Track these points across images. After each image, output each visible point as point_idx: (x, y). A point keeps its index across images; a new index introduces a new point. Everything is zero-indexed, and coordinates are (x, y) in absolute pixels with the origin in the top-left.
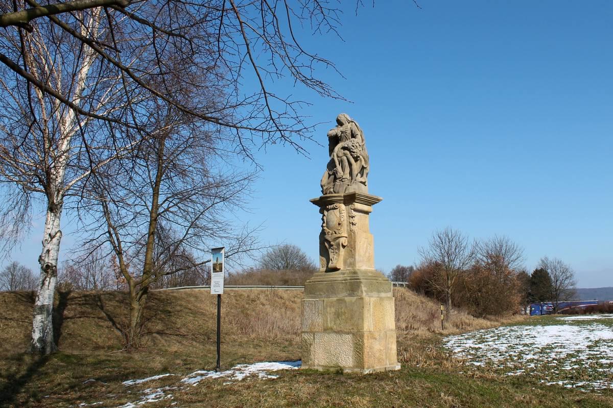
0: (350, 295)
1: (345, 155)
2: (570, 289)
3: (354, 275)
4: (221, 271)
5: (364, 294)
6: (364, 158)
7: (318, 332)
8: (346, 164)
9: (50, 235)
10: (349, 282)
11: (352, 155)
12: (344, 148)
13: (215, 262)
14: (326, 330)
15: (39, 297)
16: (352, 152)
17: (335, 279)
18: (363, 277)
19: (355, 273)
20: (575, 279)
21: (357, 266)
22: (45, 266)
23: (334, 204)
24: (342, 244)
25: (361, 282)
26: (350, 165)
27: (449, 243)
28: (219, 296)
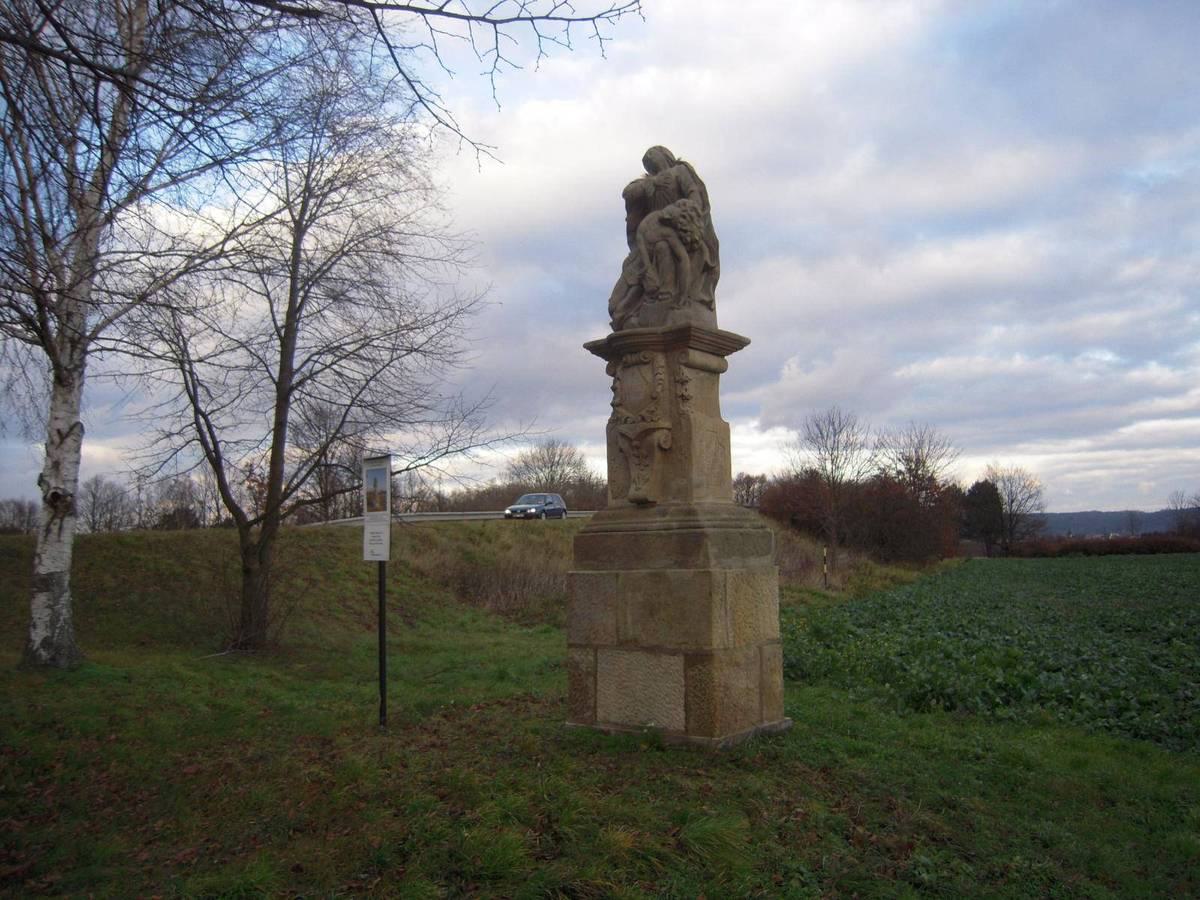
0: (681, 564)
1: (665, 238)
2: (1034, 515)
3: (687, 518)
4: (385, 509)
5: (713, 562)
6: (707, 244)
7: (605, 646)
8: (667, 259)
9: (59, 431)
10: (677, 534)
11: (681, 238)
12: (663, 222)
13: (371, 487)
14: (627, 644)
15: (40, 558)
16: (681, 230)
17: (643, 525)
18: (709, 523)
19: (691, 512)
20: (1045, 496)
21: (695, 495)
22: (49, 495)
23: (640, 351)
24: (660, 447)
25: (703, 535)
26: (676, 258)
27: (835, 436)
28: (382, 564)
